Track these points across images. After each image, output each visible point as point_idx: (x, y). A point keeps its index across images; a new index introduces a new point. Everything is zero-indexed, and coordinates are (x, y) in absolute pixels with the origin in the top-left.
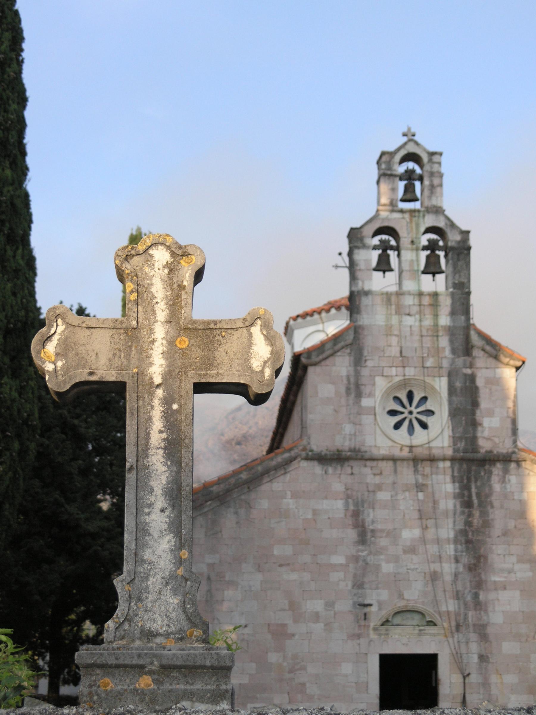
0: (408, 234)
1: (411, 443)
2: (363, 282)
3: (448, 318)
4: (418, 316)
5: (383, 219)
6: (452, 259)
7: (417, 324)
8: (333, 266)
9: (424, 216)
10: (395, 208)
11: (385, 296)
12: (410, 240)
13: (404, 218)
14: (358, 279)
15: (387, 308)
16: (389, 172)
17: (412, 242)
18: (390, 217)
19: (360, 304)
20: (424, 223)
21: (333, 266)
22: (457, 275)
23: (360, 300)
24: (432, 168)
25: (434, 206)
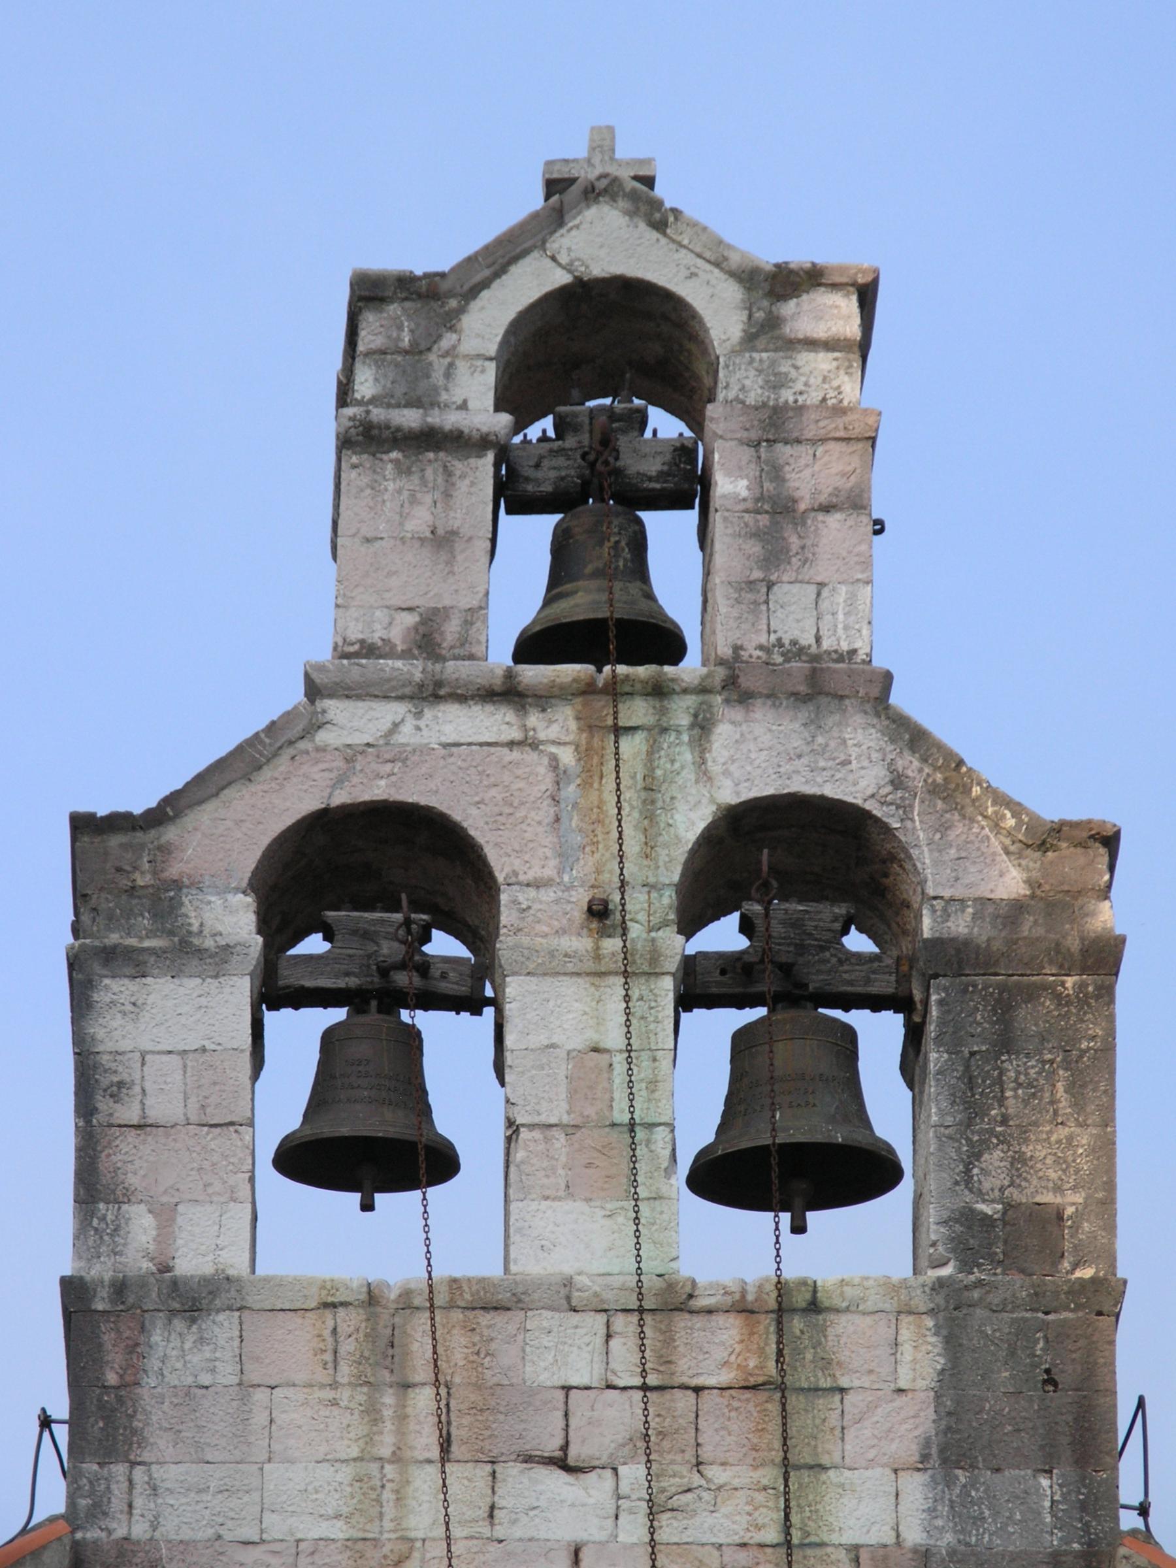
0: (565, 856)
1: (484, 1519)
2: (166, 1216)
3: (915, 1488)
4: (633, 1473)
5: (352, 754)
6: (953, 1041)
7: (633, 1530)
8: (43, 1410)
9: (702, 726)
10: (456, 670)
11: (349, 1320)
12: (582, 897)
13: (528, 743)
14: (126, 1197)
15: (372, 1413)
16: (410, 418)
17: (599, 912)
18: (407, 735)
19: (129, 1384)
20: (703, 772)
21: (43, 1410)
22: (994, 1159)
23: (134, 1349)
24: (778, 382)
25: (797, 651)
